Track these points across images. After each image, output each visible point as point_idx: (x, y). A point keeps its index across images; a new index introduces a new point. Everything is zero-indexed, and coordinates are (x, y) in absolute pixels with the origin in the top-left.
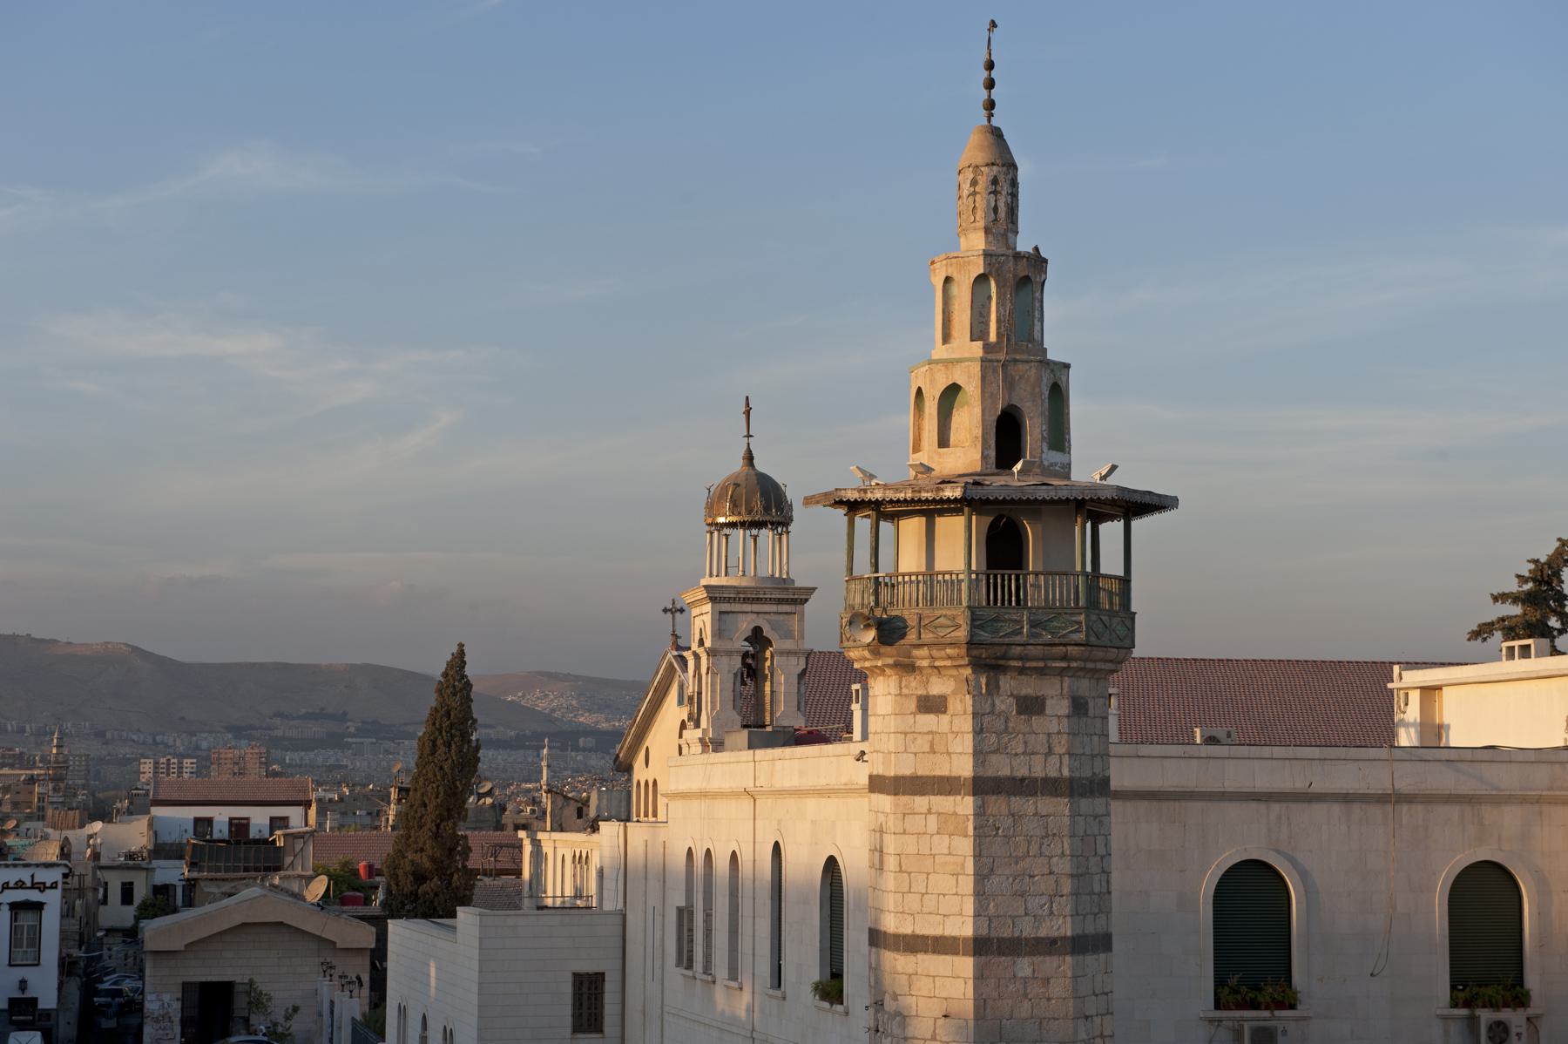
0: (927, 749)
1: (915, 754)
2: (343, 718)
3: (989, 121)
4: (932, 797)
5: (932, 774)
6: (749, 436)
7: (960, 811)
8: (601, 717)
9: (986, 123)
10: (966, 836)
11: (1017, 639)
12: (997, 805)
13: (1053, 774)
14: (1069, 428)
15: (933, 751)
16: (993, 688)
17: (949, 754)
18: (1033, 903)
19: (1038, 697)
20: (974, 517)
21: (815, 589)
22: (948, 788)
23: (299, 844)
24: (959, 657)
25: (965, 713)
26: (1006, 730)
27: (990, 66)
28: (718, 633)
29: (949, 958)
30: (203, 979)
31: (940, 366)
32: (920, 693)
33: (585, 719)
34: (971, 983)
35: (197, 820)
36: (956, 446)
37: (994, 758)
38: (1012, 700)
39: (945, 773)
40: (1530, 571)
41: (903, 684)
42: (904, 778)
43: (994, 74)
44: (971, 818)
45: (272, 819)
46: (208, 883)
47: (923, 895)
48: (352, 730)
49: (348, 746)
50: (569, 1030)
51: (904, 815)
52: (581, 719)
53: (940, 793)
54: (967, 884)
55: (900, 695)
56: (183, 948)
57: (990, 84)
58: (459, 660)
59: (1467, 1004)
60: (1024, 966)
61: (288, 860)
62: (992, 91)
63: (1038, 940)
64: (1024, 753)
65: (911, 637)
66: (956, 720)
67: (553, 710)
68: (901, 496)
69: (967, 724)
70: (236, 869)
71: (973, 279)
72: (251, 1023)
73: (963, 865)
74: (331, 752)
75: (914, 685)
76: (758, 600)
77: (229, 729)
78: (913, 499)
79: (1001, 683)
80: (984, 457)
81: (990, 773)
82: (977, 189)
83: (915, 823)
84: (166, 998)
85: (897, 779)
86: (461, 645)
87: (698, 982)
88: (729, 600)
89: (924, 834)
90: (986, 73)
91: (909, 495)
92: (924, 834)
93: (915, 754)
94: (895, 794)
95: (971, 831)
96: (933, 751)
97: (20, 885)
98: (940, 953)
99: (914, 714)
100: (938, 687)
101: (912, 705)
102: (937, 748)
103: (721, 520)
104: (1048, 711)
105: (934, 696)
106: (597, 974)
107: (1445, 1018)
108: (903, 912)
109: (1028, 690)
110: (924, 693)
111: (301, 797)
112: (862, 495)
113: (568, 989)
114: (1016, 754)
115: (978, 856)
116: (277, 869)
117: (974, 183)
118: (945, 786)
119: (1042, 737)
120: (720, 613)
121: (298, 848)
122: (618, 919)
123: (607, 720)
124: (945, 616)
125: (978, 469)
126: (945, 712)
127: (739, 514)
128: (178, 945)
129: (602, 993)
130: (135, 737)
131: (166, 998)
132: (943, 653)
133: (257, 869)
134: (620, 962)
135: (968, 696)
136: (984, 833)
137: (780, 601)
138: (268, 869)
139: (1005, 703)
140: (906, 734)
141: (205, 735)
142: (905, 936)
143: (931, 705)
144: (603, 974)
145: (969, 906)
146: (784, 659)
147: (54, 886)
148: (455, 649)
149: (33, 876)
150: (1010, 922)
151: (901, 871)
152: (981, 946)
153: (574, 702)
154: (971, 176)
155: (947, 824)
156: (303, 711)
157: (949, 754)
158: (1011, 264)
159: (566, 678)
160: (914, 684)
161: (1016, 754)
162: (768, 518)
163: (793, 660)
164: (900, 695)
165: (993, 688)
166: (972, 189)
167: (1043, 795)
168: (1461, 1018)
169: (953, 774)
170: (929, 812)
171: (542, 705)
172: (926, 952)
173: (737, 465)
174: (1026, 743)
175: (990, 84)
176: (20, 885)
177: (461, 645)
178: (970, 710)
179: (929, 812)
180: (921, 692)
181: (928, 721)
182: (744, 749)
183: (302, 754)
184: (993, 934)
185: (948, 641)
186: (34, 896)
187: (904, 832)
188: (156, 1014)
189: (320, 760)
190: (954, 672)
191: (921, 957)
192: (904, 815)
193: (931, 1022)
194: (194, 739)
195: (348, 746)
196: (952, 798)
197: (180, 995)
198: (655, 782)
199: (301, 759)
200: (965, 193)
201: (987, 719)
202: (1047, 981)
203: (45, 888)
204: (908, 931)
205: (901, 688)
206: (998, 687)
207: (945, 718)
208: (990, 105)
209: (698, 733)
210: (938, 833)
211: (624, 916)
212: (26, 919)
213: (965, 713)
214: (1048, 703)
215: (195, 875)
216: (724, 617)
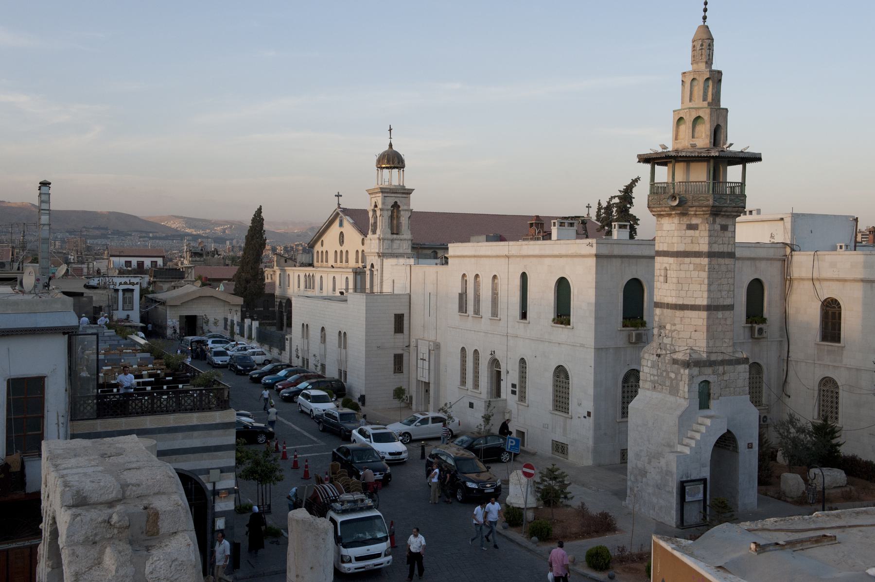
0: (690, 242)
1: (685, 244)
2: (107, 229)
3: (704, 23)
4: (692, 258)
5: (692, 250)
6: (391, 138)
7: (702, 263)
8: (193, 230)
9: (703, 24)
10: (705, 271)
11: (726, 205)
12: (715, 261)
13: (730, 251)
15: (692, 243)
16: (714, 222)
17: (699, 244)
18: (724, 293)
19: (726, 225)
21: (414, 189)
22: (698, 255)
23: (190, 270)
24: (708, 211)
25: (706, 230)
26: (717, 236)
28: (383, 203)
29: (697, 312)
30: (186, 314)
31: (693, 110)
32: (687, 223)
33: (188, 231)
34: (705, 320)
35: (126, 262)
36: (697, 138)
37: (714, 245)
38: (719, 226)
40: (624, 189)
41: (681, 220)
42: (680, 252)
44: (707, 265)
45: (126, 262)
46: (159, 283)
47: (687, 291)
48: (110, 233)
49: (109, 238)
50: (393, 332)
51: (680, 264)
52: (187, 231)
53: (695, 257)
54: (705, 287)
55: (680, 223)
56: (180, 304)
57: (705, 10)
58: (259, 211)
59: (751, 323)
61: (186, 275)
62: (706, 13)
63: (724, 306)
64: (723, 244)
65: (689, 204)
66: (702, 232)
67: (177, 228)
68: (693, 155)
69: (706, 234)
70: (169, 278)
71: (704, 80)
72: (204, 328)
73: (704, 281)
74: (103, 240)
75: (685, 221)
76: (396, 193)
77: (67, 232)
78: (698, 156)
79: (717, 220)
80: (710, 142)
81: (713, 250)
82: (703, 47)
83: (685, 267)
84: (174, 321)
85: (677, 252)
86: (261, 206)
87: (470, 317)
88: (387, 193)
89: (688, 271)
91: (696, 154)
92: (688, 271)
93: (685, 244)
94: (677, 257)
95: (707, 270)
96: (692, 243)
97: (125, 283)
98: (693, 310)
99: (685, 230)
100: (695, 221)
101: (685, 227)
102: (693, 242)
103: (384, 166)
104: (729, 230)
105: (693, 224)
106: (401, 314)
107: (744, 327)
108: (679, 297)
109: (723, 223)
110: (689, 223)
111: (161, 255)
112: (677, 154)
113: (393, 319)
114: (720, 244)
115: (709, 278)
116: (183, 278)
117: (702, 45)
118: (698, 254)
119: (727, 238)
120: (385, 196)
121: (189, 271)
122: (408, 297)
123: (195, 231)
124: (703, 197)
125: (708, 146)
126: (697, 230)
127: (390, 164)
128: (179, 304)
129: (403, 320)
130: (34, 234)
131: (174, 321)
132: (701, 210)
133: (176, 278)
134: (409, 310)
135: (707, 225)
136: (711, 270)
137: (403, 193)
138: (180, 278)
139: (717, 227)
140: (681, 237)
141: (59, 234)
142: (680, 305)
143: (691, 227)
144: (403, 314)
145: (705, 295)
146: (404, 212)
147: (137, 284)
148: (259, 207)
149: (130, 280)
150: (717, 300)
151: (678, 283)
153: (184, 225)
154: (701, 43)
155: (698, 268)
156: (93, 226)
157: (699, 244)
158: (717, 75)
159: (181, 217)
160: (685, 220)
161: (720, 244)
162: (399, 166)
163: (407, 212)
164: (680, 223)
165: (714, 222)
166: (701, 47)
167: (727, 258)
168: (748, 327)
169: (700, 250)
170: (690, 263)
171: (173, 226)
172: (688, 310)
173: (387, 148)
174: (723, 240)
175: (705, 10)
176: (125, 283)
177: (261, 206)
178: (707, 229)
179: (690, 263)
180: (688, 223)
181: (691, 233)
182: (484, 241)
183: (93, 240)
184: (712, 304)
185: (704, 205)
186: (131, 287)
187: (680, 270)
188: (171, 326)
189: (99, 243)
190: (702, 216)
191: (685, 311)
192: (680, 264)
193: (689, 333)
194: (55, 235)
195: (109, 238)
196: (699, 259)
197: (179, 320)
199: (93, 242)
200: (698, 49)
201: (712, 232)
202: (726, 319)
203: (134, 284)
204: (681, 303)
205: (680, 221)
206: (716, 222)
207: (697, 232)
208: (705, 18)
209: (376, 236)
210: (694, 270)
211: (410, 296)
212: (128, 295)
213: (706, 230)
214: (729, 227)
215: (155, 280)
216: (385, 198)
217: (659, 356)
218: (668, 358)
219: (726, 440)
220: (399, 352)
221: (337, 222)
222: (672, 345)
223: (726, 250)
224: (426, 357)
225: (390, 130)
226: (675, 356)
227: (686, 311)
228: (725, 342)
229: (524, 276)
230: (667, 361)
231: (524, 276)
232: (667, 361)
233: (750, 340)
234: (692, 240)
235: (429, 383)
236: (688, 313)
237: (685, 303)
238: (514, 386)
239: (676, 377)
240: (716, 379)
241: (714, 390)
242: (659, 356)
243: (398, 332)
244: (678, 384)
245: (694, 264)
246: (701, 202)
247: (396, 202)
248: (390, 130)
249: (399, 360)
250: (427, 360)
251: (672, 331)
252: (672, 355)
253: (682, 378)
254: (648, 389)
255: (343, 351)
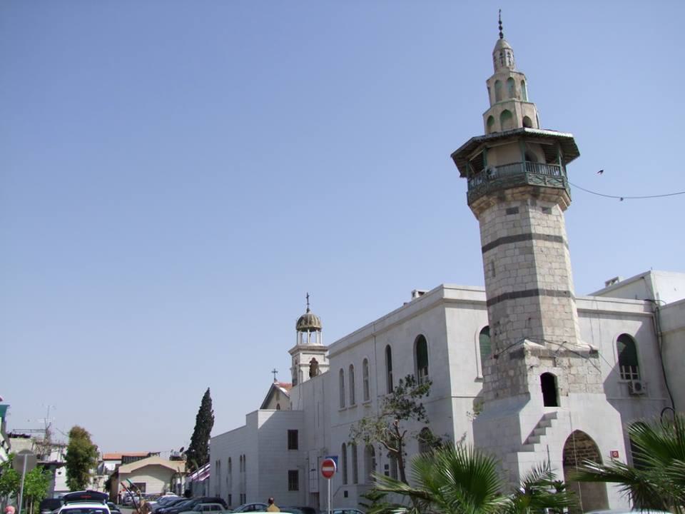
0: (512, 226)
14: (466, 144)
15: (514, 226)
20: (101, 511)
27: (500, 23)
29: (529, 298)
39: (520, 233)
43: (502, 25)
58: (208, 392)
60: (555, 300)
75: (504, 206)
90: (499, 31)
99: (505, 215)
100: (513, 205)
101: (505, 212)
126: (518, 213)
140: (503, 223)
142: (510, 293)
148: (207, 389)
152: (529, 237)
170: (515, 248)
179: (515, 248)
180: (507, 207)
181: (512, 217)
198: (244, 456)
217: (496, 357)
218: (506, 356)
219: (587, 452)
220: (294, 468)
221: (275, 396)
222: (508, 339)
223: (552, 234)
224: (316, 467)
225: (307, 297)
226: (511, 350)
227: (518, 299)
228: (566, 331)
229: (389, 350)
230: (505, 359)
231: (389, 350)
232: (505, 359)
233: (629, 398)
234: (514, 224)
235: (318, 493)
236: (519, 300)
237: (515, 290)
238: (386, 467)
239: (515, 373)
240: (561, 372)
241: (561, 384)
242: (496, 357)
243: (293, 449)
244: (518, 381)
245: (519, 248)
246: (516, 183)
247: (314, 359)
248: (307, 297)
249: (293, 476)
250: (316, 469)
251: (505, 325)
252: (509, 350)
253: (520, 371)
254: (492, 400)
255: (243, 473)
